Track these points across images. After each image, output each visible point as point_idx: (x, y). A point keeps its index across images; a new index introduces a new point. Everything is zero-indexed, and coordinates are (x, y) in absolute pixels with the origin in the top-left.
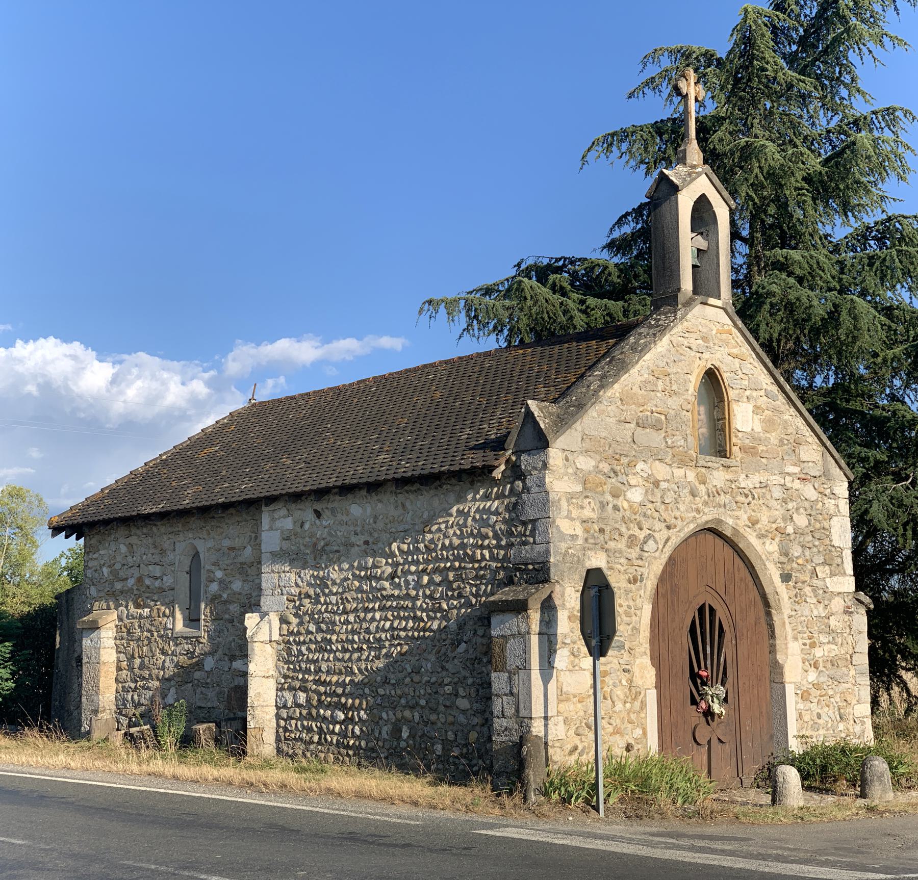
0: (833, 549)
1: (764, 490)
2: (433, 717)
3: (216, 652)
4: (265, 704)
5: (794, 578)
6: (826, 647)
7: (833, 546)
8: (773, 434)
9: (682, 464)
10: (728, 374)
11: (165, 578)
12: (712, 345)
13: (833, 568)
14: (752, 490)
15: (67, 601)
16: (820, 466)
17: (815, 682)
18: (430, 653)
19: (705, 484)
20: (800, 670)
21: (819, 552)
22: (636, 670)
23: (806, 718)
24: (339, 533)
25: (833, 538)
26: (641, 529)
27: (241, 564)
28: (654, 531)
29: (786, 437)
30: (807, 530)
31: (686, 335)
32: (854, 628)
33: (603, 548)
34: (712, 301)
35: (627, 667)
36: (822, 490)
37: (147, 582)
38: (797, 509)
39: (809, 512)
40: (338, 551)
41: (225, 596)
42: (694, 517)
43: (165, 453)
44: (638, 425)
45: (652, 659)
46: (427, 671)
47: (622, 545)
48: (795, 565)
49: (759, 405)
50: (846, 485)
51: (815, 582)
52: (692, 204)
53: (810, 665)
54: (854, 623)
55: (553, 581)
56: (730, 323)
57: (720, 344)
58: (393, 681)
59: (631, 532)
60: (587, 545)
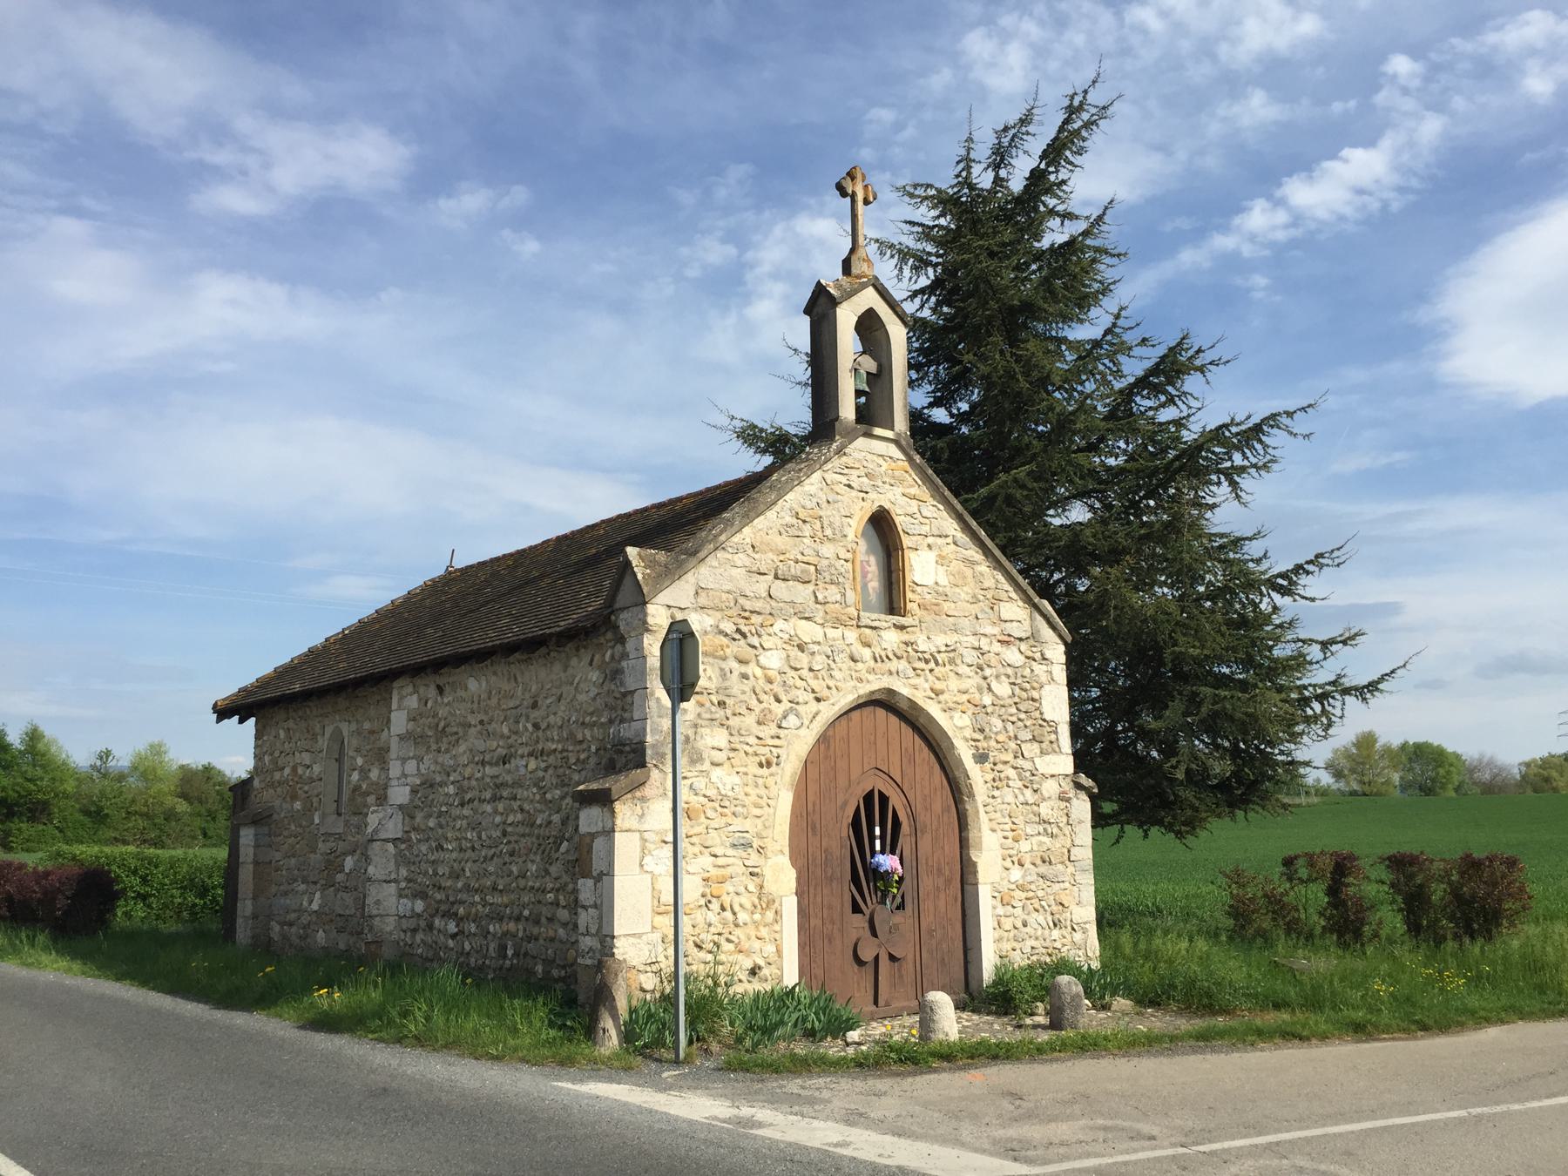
0: (1045, 724)
1: (952, 655)
2: (535, 931)
3: (355, 851)
4: (385, 913)
5: (992, 759)
6: (1035, 840)
7: (1044, 720)
8: (965, 588)
9: (839, 622)
10: (903, 517)
11: (314, 767)
12: (880, 484)
13: (1044, 745)
14: (936, 654)
15: (242, 794)
16: (1027, 624)
17: (1021, 882)
18: (535, 853)
19: (869, 646)
20: (1001, 869)
21: (1026, 726)
22: (767, 872)
23: (1007, 924)
24: (458, 712)
25: (1044, 710)
26: (778, 701)
27: (380, 749)
28: (797, 703)
29: (982, 592)
30: (1011, 701)
31: (846, 471)
32: (1073, 816)
33: (722, 725)
34: (878, 431)
35: (756, 870)
36: (1030, 654)
37: (300, 771)
38: (997, 677)
39: (1012, 680)
40: (456, 733)
41: (364, 787)
42: (855, 687)
43: (348, 628)
44: (776, 577)
45: (790, 859)
46: (532, 874)
47: (750, 720)
48: (993, 743)
49: (944, 554)
50: (1062, 648)
51: (1020, 762)
52: (856, 319)
53: (1013, 862)
54: (1073, 810)
55: (649, 765)
56: (902, 457)
57: (892, 482)
58: (501, 887)
59: (765, 705)
60: (700, 722)
